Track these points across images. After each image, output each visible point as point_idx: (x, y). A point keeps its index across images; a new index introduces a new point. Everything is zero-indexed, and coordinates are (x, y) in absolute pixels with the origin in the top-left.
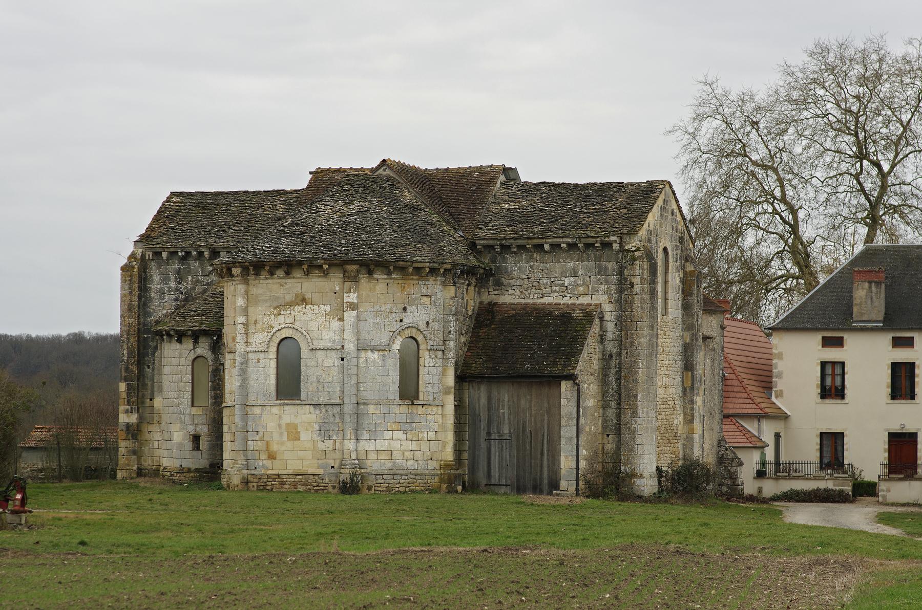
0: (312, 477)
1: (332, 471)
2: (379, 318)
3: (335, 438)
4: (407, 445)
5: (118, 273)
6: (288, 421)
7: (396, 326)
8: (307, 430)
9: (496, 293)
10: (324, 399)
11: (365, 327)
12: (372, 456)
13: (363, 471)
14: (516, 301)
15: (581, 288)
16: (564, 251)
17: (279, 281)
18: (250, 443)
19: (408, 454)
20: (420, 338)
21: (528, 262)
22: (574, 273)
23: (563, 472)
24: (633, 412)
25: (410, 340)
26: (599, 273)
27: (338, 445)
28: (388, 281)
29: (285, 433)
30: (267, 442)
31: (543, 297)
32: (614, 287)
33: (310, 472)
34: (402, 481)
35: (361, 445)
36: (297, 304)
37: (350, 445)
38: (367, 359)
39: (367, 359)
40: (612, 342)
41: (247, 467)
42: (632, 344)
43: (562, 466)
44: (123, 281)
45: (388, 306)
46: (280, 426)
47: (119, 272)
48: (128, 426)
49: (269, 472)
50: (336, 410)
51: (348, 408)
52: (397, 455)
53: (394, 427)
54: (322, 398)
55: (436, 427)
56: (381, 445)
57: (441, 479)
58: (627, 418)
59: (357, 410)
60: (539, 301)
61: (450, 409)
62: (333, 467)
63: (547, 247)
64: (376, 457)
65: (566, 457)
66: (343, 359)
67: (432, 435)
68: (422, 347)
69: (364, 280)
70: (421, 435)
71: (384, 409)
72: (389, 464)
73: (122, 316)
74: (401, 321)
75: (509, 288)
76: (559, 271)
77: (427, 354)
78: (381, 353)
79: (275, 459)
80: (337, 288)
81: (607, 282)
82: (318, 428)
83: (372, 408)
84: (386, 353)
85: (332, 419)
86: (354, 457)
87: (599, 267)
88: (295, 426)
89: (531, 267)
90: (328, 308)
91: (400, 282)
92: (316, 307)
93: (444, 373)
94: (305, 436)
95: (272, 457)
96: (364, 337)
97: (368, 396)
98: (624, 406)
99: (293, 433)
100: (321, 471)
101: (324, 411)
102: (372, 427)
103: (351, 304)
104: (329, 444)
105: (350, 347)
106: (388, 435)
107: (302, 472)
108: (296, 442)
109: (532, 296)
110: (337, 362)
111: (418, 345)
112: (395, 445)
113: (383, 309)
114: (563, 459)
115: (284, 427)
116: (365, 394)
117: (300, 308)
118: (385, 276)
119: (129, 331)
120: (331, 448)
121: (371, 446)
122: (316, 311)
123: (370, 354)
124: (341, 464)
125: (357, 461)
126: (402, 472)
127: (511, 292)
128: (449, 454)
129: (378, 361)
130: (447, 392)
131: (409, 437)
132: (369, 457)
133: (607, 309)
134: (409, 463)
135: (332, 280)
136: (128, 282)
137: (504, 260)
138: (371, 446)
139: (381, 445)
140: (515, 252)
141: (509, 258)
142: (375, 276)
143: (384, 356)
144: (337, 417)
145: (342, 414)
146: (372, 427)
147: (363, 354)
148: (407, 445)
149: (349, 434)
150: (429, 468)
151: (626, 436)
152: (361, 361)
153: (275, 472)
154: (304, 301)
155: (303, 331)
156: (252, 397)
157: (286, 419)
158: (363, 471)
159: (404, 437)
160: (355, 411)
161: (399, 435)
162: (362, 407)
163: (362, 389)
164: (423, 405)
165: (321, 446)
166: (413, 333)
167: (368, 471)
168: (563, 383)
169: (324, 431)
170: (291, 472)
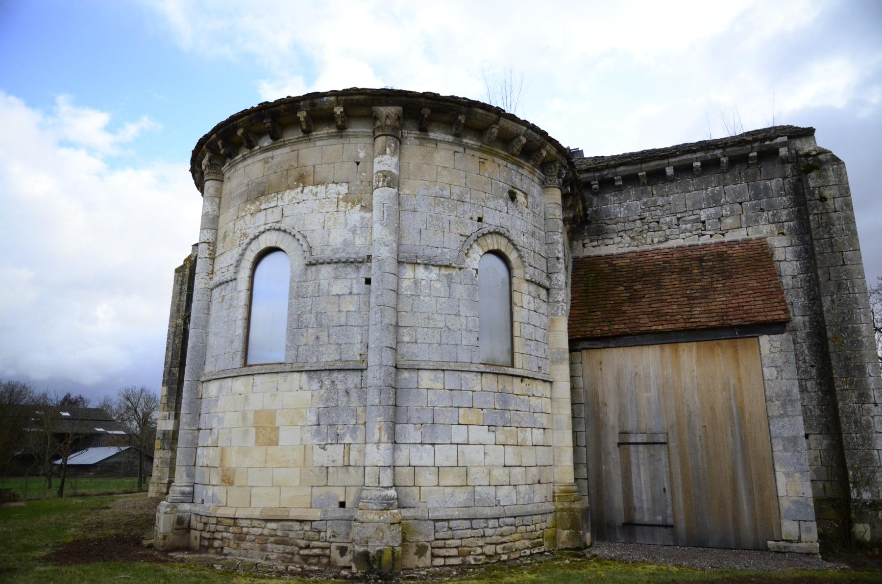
0: (297, 526)
1: (340, 513)
2: (439, 209)
3: (348, 439)
4: (497, 455)
5: (172, 275)
6: (259, 407)
7: (472, 228)
8: (292, 424)
9: (595, 243)
10: (329, 356)
11: (412, 223)
12: (427, 479)
13: (405, 513)
14: (626, 250)
15: (729, 221)
16: (671, 180)
17: (264, 156)
18: (199, 450)
19: (500, 474)
20: (513, 256)
21: (639, 199)
22: (715, 201)
23: (785, 504)
24: (861, 395)
25: (493, 259)
26: (757, 197)
27: (354, 456)
28: (457, 148)
29: (253, 431)
30: (223, 450)
31: (667, 240)
32: (785, 212)
33: (293, 514)
34: (489, 532)
35: (405, 455)
36: (289, 188)
37: (377, 454)
38: (416, 282)
39: (416, 282)
40: (792, 292)
41: (190, 497)
42: (839, 286)
43: (781, 492)
44: (176, 281)
45: (456, 191)
46: (244, 418)
47: (173, 274)
48: (165, 433)
49: (221, 512)
50: (353, 379)
51: (375, 375)
52: (478, 477)
53: (472, 416)
54: (324, 359)
55: (543, 420)
56: (445, 455)
57: (556, 519)
58: (848, 402)
59: (396, 380)
60: (662, 246)
61: (563, 388)
62: (342, 505)
63: (670, 171)
64: (433, 480)
65: (787, 475)
66: (368, 281)
67: (538, 436)
68: (517, 272)
69: (411, 135)
70: (521, 435)
71: (451, 380)
72: (461, 496)
73: (171, 317)
74: (480, 220)
75: (614, 235)
76: (689, 203)
77: (525, 287)
78: (444, 271)
79: (231, 483)
80: (362, 155)
81: (771, 207)
82: (313, 419)
83: (426, 379)
84: (454, 272)
85: (342, 401)
86: (386, 481)
87: (756, 189)
88: (271, 415)
89: (644, 204)
90: (343, 189)
91: (478, 154)
92: (321, 188)
93: (549, 329)
94: (288, 437)
95: (228, 480)
96: (410, 240)
97: (421, 353)
98: (839, 384)
99: (266, 432)
100: (316, 514)
101: (327, 383)
102: (427, 418)
103: (385, 174)
104: (336, 453)
105: (384, 253)
106: (459, 434)
107: (278, 514)
108: (272, 449)
109: (649, 241)
110: (359, 286)
111: (509, 269)
112: (473, 454)
113: (446, 193)
114: (781, 479)
115: (251, 416)
116: (414, 348)
117: (293, 193)
118: (450, 138)
119: (175, 332)
120: (340, 462)
121: (423, 456)
122: (322, 195)
123: (421, 272)
124: (359, 498)
125: (392, 493)
126: (488, 512)
127: (617, 240)
128: (564, 472)
129: (438, 285)
130: (556, 361)
131: (501, 438)
132: (420, 481)
133: (776, 244)
134: (503, 492)
135: (353, 140)
136: (180, 283)
137: (605, 202)
138: (423, 456)
139: (445, 455)
140: (619, 186)
141: (611, 197)
142: (432, 135)
143: (449, 278)
144: (354, 394)
145: (362, 388)
146: (427, 418)
147: (408, 272)
148: (497, 455)
149: (377, 429)
150: (537, 499)
151: (852, 437)
152: (405, 284)
153: (229, 512)
154: (302, 180)
155: (294, 232)
156: (209, 368)
157: (257, 402)
158: (405, 513)
159: (489, 437)
160: (390, 381)
161: (480, 433)
162: (406, 375)
163: (406, 339)
164: (523, 378)
165: (320, 457)
166: (501, 244)
167: (418, 513)
168: (764, 340)
169: (328, 426)
170: (256, 514)
